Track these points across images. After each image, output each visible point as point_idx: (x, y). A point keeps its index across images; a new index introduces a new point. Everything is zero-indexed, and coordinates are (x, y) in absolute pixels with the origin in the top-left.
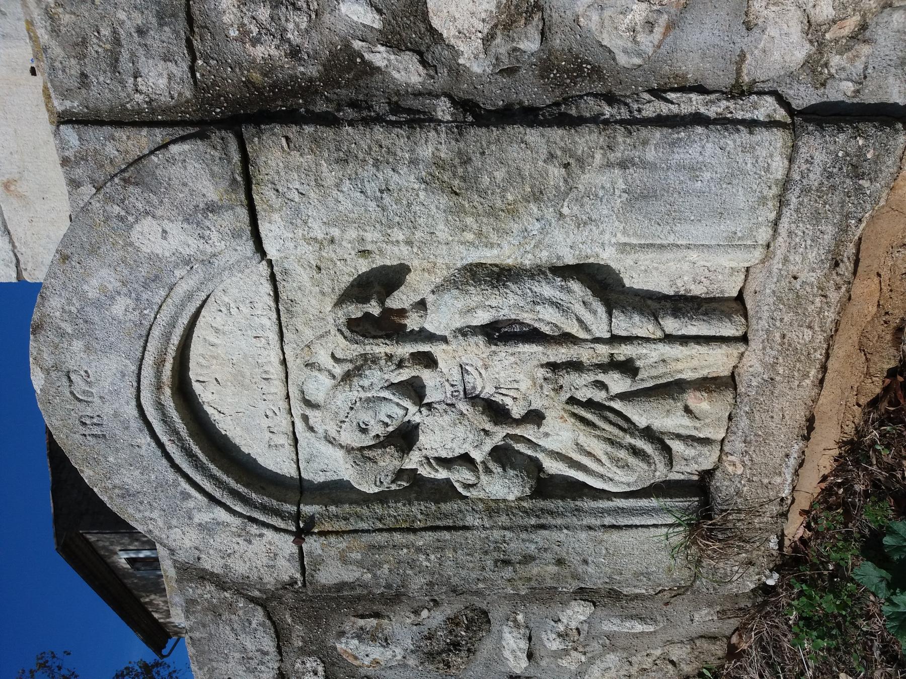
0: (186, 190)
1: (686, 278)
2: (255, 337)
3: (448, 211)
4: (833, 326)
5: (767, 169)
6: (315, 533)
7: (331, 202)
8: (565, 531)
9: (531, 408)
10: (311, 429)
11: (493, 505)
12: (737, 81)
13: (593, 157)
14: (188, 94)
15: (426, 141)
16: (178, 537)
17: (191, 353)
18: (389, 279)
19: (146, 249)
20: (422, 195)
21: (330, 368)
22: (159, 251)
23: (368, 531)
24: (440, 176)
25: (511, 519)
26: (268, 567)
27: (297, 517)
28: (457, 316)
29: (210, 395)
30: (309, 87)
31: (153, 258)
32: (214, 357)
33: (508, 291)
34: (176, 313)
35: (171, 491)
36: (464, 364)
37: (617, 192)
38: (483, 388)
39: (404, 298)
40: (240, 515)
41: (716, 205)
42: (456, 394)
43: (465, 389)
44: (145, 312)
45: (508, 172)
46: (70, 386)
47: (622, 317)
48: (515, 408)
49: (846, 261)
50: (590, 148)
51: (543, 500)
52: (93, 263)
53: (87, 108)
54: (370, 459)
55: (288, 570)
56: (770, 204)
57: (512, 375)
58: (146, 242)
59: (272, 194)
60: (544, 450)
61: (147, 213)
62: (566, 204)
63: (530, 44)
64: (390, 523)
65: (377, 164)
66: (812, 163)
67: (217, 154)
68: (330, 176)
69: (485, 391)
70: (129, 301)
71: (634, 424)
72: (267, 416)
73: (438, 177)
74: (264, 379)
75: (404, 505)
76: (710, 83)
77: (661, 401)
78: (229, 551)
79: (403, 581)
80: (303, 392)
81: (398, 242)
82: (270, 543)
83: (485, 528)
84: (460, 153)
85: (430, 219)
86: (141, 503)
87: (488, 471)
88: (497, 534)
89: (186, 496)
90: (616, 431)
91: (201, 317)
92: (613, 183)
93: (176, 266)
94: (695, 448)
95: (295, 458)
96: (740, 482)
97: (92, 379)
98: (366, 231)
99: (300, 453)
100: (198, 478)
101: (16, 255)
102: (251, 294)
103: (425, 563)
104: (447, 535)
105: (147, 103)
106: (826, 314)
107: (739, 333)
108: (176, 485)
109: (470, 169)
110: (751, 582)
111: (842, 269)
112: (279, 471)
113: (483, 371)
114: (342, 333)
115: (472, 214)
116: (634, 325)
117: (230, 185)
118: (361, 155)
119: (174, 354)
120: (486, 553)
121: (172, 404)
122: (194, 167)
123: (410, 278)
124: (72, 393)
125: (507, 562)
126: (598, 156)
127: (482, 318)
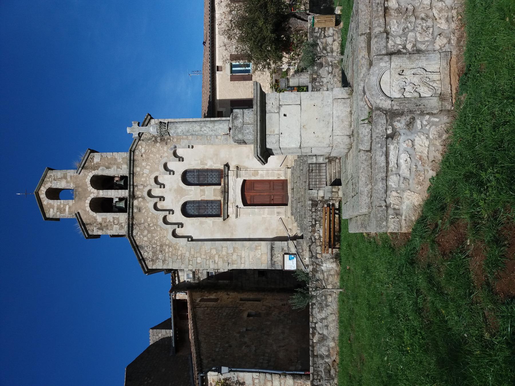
18: (403, 71)
55: (390, 107)
57: (416, 80)
63: (415, 48)
73: (408, 58)
127: (413, 72)
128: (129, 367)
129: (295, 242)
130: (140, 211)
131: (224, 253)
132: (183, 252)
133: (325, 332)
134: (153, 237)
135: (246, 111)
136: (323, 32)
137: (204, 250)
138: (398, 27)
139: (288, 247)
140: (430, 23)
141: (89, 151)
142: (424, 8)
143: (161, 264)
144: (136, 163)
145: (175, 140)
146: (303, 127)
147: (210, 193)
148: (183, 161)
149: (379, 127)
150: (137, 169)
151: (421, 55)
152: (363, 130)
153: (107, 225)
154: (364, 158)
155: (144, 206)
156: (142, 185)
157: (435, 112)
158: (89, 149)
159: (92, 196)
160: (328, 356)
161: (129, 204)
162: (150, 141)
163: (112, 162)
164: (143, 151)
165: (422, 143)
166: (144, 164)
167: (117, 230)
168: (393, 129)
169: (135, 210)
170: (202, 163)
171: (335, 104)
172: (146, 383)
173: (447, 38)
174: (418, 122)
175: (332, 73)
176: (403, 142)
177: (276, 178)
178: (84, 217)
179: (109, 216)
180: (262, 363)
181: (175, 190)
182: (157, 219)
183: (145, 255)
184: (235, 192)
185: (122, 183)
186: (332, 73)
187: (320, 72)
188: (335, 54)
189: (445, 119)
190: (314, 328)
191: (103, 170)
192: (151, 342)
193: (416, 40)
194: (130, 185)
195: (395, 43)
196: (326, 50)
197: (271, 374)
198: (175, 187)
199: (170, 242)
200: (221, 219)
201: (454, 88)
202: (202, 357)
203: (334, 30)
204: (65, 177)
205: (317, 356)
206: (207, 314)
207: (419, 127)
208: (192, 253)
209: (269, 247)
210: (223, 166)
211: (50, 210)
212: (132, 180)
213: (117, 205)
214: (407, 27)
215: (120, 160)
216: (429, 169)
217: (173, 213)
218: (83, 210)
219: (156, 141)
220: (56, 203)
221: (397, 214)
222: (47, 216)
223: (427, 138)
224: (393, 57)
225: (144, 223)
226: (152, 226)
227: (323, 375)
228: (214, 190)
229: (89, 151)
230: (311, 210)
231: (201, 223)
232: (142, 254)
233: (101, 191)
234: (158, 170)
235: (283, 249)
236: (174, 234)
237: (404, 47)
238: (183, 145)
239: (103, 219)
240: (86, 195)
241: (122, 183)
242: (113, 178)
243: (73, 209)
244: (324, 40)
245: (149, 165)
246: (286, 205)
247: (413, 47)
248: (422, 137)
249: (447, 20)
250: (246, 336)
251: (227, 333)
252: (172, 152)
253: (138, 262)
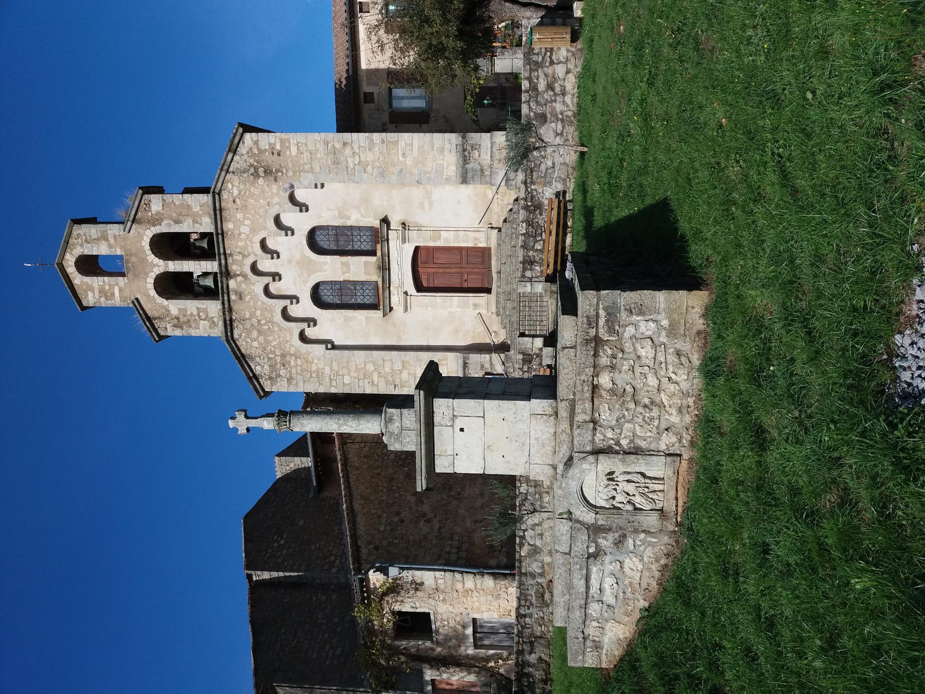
36: (623, 486)
57: (630, 488)
128: (247, 518)
129: (502, 355)
130: (241, 298)
131: (387, 369)
132: (321, 366)
133: (538, 543)
134: (268, 342)
135: (405, 411)
136: (548, 54)
137: (354, 363)
138: (610, 414)
139: (491, 364)
140: (655, 412)
141: (141, 191)
142: (648, 391)
143: (285, 383)
144: (225, 214)
145: (291, 174)
146: (487, 448)
147: (358, 269)
148: (307, 210)
149: (579, 544)
150: (229, 226)
152: (561, 527)
153: (189, 321)
154: (561, 561)
155: (247, 290)
156: (240, 253)
158: (140, 188)
159: (157, 271)
160: (542, 575)
161: (222, 287)
162: (245, 175)
163: (184, 212)
164: (236, 192)
165: (632, 564)
166: (239, 216)
167: (205, 329)
168: (597, 546)
169: (233, 297)
170: (341, 215)
171: (534, 422)
172: (276, 545)
173: (676, 434)
174: (631, 541)
175: (561, 134)
176: (609, 564)
177: (471, 245)
178: (147, 307)
179: (191, 306)
180: (449, 553)
181: (297, 262)
182: (271, 311)
183: (258, 370)
184: (400, 269)
185: (205, 244)
186: (561, 134)
187: (542, 132)
188: (568, 99)
189: (666, 539)
190: (523, 537)
191: (169, 225)
192: (279, 475)
193: (634, 435)
194: (219, 255)
195: (605, 436)
196: (553, 89)
197: (462, 573)
198: (298, 256)
199: (297, 350)
200: (378, 314)
201: (680, 503)
202: (360, 543)
203: (568, 51)
204: (104, 237)
205: (525, 574)
206: (366, 457)
207: (632, 548)
208: (336, 368)
209: (461, 362)
210: (378, 222)
211: (87, 295)
212: (221, 245)
213: (201, 283)
214: (624, 416)
215: (196, 209)
216: (640, 598)
217: (298, 302)
218: (145, 294)
219: (256, 175)
220: (96, 282)
221: (596, 647)
222: (85, 304)
223: (640, 560)
224: (601, 457)
225: (250, 319)
226: (265, 324)
227: (534, 601)
228: (366, 263)
229: (141, 191)
230: (521, 369)
231: (347, 319)
232: (253, 367)
233: (170, 263)
234: (265, 228)
235: (482, 367)
236: (303, 338)
237: (618, 443)
238: (306, 183)
239: (180, 310)
240: (147, 269)
241: (205, 244)
242: (187, 235)
243: (127, 293)
244: (550, 71)
245: (248, 219)
246: (488, 291)
247: (629, 443)
248: (634, 559)
249: (680, 410)
250: (425, 501)
251: (397, 495)
252: (287, 194)
253: (248, 381)
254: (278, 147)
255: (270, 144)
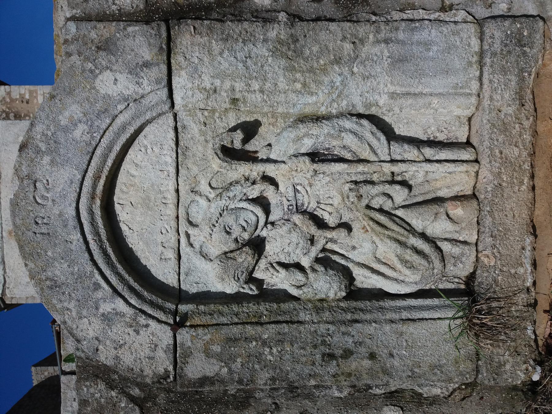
0: (133, 54)
1: (433, 129)
2: (161, 171)
3: (286, 69)
4: (531, 146)
5: (469, 45)
6: (187, 326)
7: (216, 63)
8: (374, 324)
9: (342, 221)
10: (191, 245)
11: (319, 304)
12: (443, 5)
13: (368, 38)
14: (142, 6)
15: (273, 29)
16: (85, 327)
17: (118, 181)
18: (250, 130)
19: (102, 92)
20: (270, 59)
21: (208, 194)
22: (110, 93)
23: (227, 325)
24: (281, 49)
25: (333, 315)
26: (149, 358)
27: (175, 313)
28: (291, 144)
29: (125, 215)
30: (208, 7)
31: (106, 97)
32: (132, 185)
33: (323, 125)
34: (113, 139)
35: (87, 283)
37: (385, 58)
38: (309, 203)
39: (257, 143)
40: (134, 307)
41: (444, 66)
42: (291, 207)
43: (296, 204)
44: (95, 135)
45: (320, 48)
46: (35, 191)
47: (397, 145)
48: (331, 219)
49: (528, 100)
50: (366, 33)
51: (356, 301)
52: (69, 100)
53: (85, 14)
54: (231, 258)
55: (164, 363)
56: (475, 66)
57: (327, 191)
58: (103, 86)
59: (181, 59)
60: (353, 261)
61: (107, 68)
62: (355, 65)
64: (243, 317)
65: (244, 42)
66: (494, 38)
67: (154, 32)
68: (216, 47)
69: (311, 206)
70: (86, 127)
71: (414, 229)
72: (162, 233)
74: (164, 203)
75: (254, 305)
76: (427, 7)
77: (430, 207)
78: (121, 342)
79: (252, 376)
80: (188, 214)
81: (255, 91)
82: (153, 334)
83: (313, 323)
84: (292, 35)
85: (275, 74)
86: (63, 293)
87: (314, 270)
88: (322, 328)
89: (97, 287)
90: (402, 231)
91: (128, 155)
92: (382, 52)
93: (119, 102)
94: (459, 246)
95: (177, 270)
96: (495, 272)
97: (50, 186)
98: (236, 82)
99: (181, 267)
100: (108, 273)
101: (5, 278)
102: (162, 139)
103: (269, 357)
104: (285, 328)
105: (118, 10)
106: (525, 136)
107: (472, 158)
108: (92, 275)
109: (298, 45)
110: (521, 371)
111: (527, 107)
112: (165, 281)
113: (308, 189)
114: (217, 155)
115: (300, 71)
116: (405, 151)
117: (159, 51)
118: (235, 36)
119: (107, 174)
120: (315, 347)
121: (99, 213)
122: (139, 39)
123: (262, 130)
124: (34, 197)
125: (332, 356)
126: (371, 36)
127: (307, 145)
151: (362, 30)
157: (437, 391)
192: (35, 383)
254: (27, 97)
255: (20, 94)
